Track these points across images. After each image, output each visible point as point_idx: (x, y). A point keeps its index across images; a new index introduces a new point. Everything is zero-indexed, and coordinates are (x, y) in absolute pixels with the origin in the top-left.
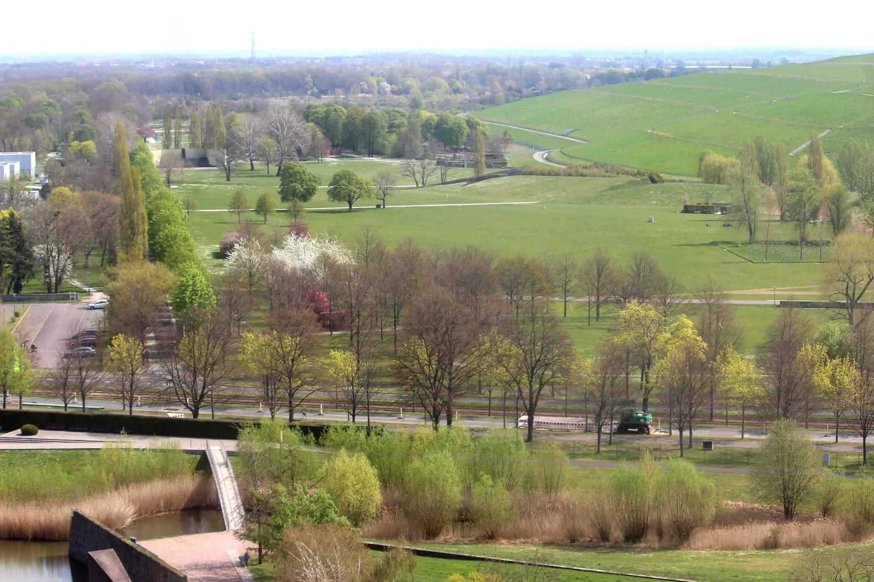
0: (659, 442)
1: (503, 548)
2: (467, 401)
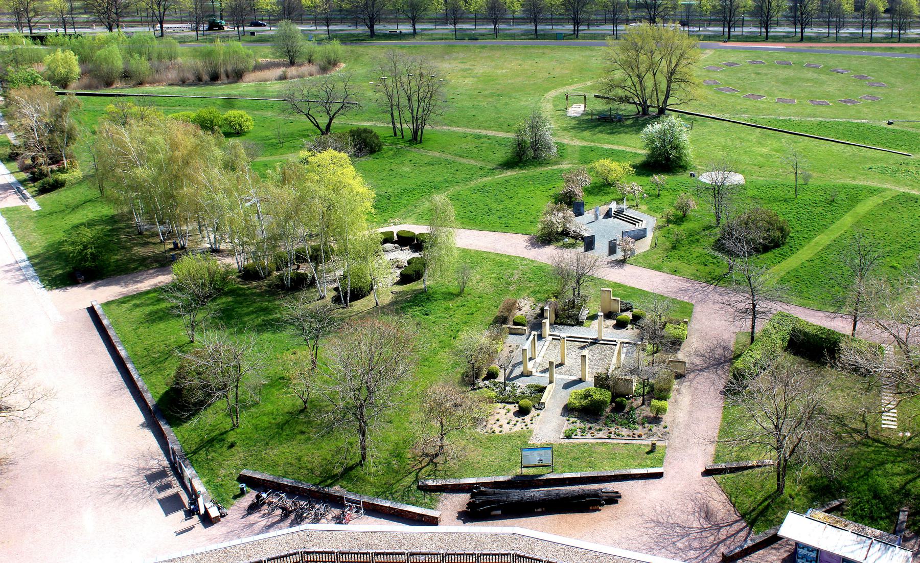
0: (229, 33)
1: (147, 89)
2: (126, 19)
